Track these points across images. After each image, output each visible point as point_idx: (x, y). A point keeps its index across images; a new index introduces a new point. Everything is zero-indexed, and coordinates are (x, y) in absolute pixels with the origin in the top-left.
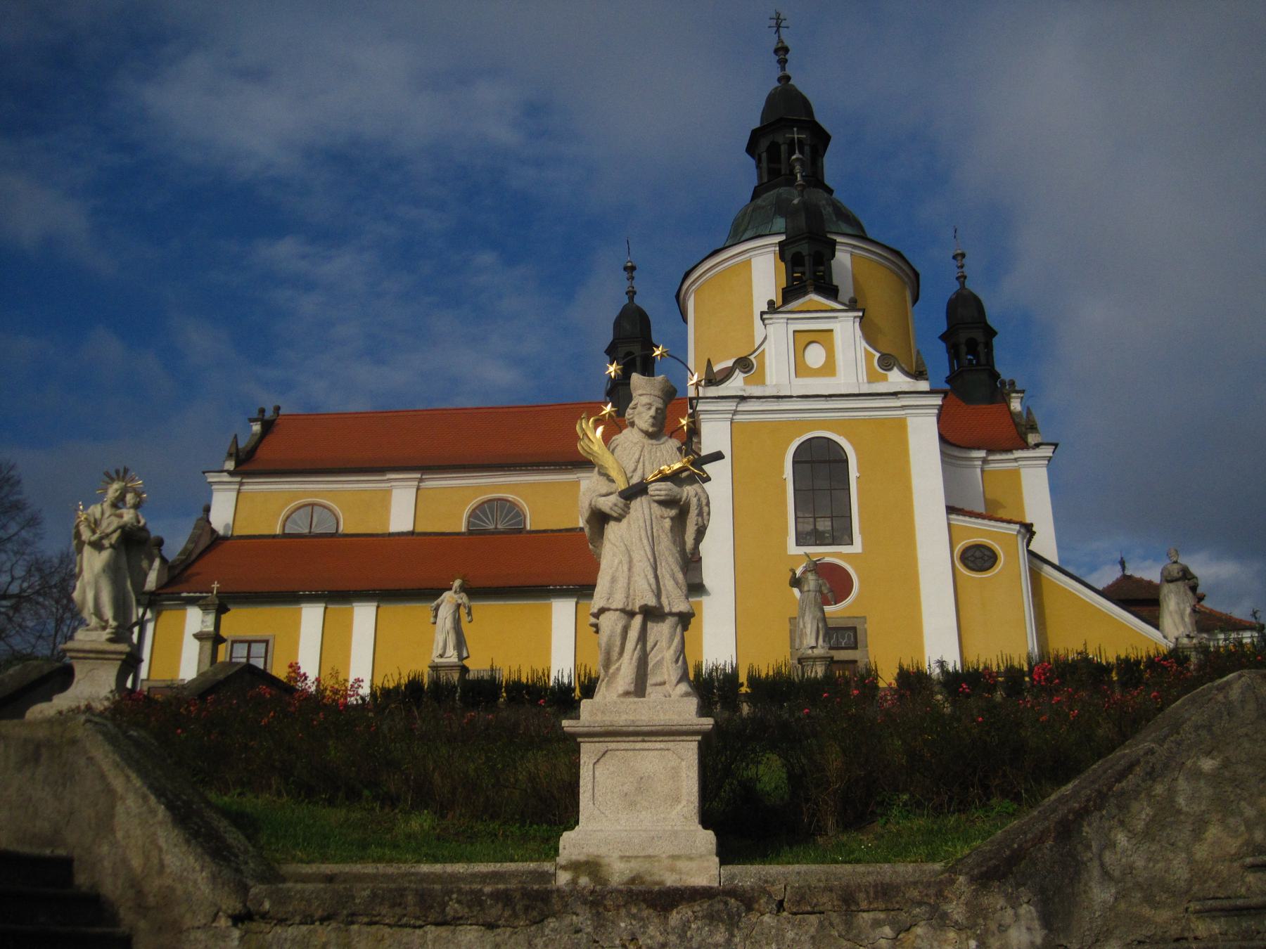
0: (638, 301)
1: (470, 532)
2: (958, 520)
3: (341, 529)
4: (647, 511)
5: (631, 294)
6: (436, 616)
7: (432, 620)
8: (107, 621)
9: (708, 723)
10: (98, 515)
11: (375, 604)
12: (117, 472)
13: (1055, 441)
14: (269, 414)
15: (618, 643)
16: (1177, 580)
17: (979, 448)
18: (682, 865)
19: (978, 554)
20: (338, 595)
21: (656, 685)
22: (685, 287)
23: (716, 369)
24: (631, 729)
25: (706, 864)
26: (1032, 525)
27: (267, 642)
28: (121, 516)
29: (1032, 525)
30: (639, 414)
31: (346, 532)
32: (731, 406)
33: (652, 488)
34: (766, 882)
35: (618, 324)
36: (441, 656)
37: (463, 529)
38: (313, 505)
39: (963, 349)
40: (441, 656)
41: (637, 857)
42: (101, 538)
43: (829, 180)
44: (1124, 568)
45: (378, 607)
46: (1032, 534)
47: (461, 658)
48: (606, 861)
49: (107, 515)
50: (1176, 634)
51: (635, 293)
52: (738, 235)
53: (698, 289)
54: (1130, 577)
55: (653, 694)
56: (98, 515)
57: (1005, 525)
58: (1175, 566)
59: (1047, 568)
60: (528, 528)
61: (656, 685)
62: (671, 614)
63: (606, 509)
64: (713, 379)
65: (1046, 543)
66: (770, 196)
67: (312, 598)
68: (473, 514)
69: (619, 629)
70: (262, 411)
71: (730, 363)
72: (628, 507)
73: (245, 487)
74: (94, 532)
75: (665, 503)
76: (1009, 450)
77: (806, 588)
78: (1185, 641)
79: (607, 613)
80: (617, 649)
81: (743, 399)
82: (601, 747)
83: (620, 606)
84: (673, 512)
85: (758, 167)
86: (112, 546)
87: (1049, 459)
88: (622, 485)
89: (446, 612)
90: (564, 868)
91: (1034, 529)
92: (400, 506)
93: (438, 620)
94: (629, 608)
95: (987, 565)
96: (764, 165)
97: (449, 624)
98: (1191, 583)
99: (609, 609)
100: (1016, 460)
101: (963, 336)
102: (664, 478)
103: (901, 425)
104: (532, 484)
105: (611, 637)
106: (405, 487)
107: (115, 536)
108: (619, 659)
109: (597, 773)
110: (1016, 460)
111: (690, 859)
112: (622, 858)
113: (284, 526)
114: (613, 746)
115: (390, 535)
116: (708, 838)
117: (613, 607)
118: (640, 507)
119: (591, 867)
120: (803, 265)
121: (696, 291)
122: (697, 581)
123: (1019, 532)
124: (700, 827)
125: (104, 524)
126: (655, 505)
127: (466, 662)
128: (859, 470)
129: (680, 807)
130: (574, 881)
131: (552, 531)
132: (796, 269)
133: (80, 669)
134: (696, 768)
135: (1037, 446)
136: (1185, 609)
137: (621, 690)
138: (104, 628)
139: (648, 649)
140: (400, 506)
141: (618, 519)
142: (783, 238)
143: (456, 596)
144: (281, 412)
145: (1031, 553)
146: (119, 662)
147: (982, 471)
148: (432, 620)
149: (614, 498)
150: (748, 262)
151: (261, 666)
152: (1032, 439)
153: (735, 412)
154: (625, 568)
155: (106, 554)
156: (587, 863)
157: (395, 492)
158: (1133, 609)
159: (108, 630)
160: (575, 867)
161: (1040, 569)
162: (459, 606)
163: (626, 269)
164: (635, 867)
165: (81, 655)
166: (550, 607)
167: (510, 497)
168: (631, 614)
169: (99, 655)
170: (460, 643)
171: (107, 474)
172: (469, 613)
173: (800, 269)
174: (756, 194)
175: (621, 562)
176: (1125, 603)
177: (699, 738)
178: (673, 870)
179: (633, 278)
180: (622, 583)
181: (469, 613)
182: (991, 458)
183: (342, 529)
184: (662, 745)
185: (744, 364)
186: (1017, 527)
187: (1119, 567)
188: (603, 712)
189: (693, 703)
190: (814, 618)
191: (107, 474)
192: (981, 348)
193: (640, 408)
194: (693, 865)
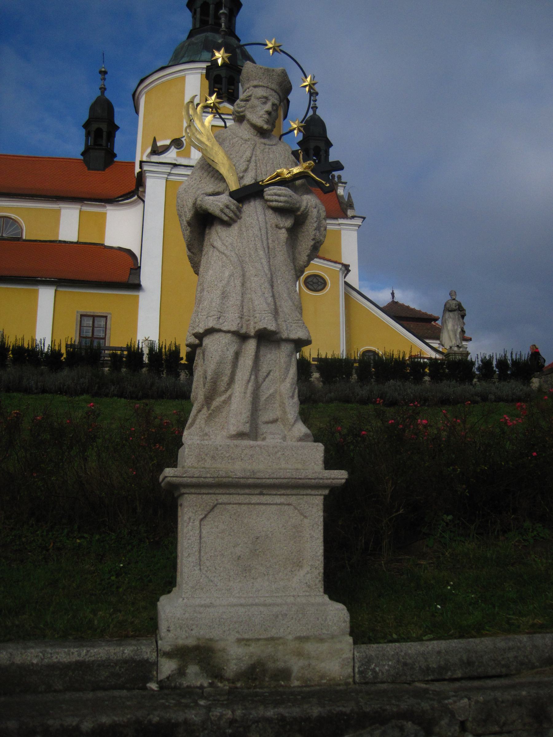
0: (107, 95)
4: (261, 218)
5: (103, 89)
9: (340, 476)
15: (228, 372)
16: (454, 310)
18: (310, 647)
19: (315, 280)
21: (267, 423)
22: (139, 89)
23: (159, 144)
24: (250, 481)
25: (338, 646)
26: (349, 266)
29: (349, 266)
30: (253, 107)
32: (167, 169)
33: (269, 193)
34: (405, 664)
35: (93, 108)
39: (312, 152)
41: (259, 640)
43: (238, 33)
46: (348, 271)
48: (221, 645)
50: (451, 344)
51: (105, 89)
52: (178, 58)
53: (148, 91)
54: (397, 303)
55: (272, 438)
58: (454, 302)
60: (24, 238)
61: (267, 423)
62: (288, 340)
63: (216, 211)
64: (156, 151)
66: (201, 37)
69: (230, 354)
71: (168, 142)
72: (239, 210)
75: (280, 211)
76: (336, 218)
78: (456, 349)
79: (217, 336)
80: (226, 379)
81: (175, 165)
82: (210, 500)
83: (234, 328)
84: (289, 223)
85: (194, 17)
87: (359, 226)
88: (234, 186)
90: (169, 655)
94: (243, 331)
95: (320, 288)
96: (198, 16)
98: (462, 313)
99: (219, 331)
100: (339, 224)
101: (312, 145)
102: (284, 182)
105: (220, 363)
108: (226, 390)
109: (204, 532)
111: (321, 640)
112: (239, 641)
114: (223, 499)
115: (60, 241)
116: (337, 614)
117: (225, 329)
118: (253, 212)
119: (201, 654)
120: (221, 84)
121: (146, 93)
122: (137, 282)
123: (341, 269)
124: (326, 597)
126: (270, 213)
129: (302, 573)
130: (181, 672)
131: (40, 241)
132: (216, 85)
134: (321, 528)
135: (353, 217)
136: (457, 329)
137: (233, 430)
139: (260, 380)
141: (227, 224)
142: (209, 64)
145: (346, 283)
149: (225, 199)
150: (183, 78)
152: (350, 213)
153: (169, 174)
154: (238, 283)
156: (197, 648)
158: (401, 322)
160: (182, 653)
163: (101, 72)
164: (256, 651)
166: (37, 291)
167: (13, 216)
168: (243, 337)
173: (219, 86)
174: (191, 35)
175: (231, 276)
176: (398, 319)
177: (326, 492)
178: (300, 654)
179: (104, 79)
180: (234, 299)
184: (282, 499)
185: (177, 143)
186: (340, 266)
188: (213, 458)
189: (317, 451)
192: (322, 153)
193: (254, 101)
194: (325, 647)
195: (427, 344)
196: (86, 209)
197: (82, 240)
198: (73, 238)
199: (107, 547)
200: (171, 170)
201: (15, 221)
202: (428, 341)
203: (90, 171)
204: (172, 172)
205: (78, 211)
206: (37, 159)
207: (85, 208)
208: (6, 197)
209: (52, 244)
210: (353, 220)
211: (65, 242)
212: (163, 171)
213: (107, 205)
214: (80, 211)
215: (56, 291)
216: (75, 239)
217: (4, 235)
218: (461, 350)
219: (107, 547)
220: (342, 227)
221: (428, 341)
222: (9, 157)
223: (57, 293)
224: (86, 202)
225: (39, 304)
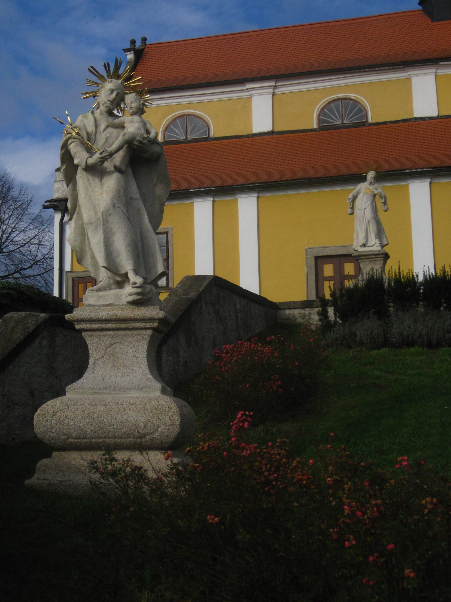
1: (321, 128)
3: (212, 134)
6: (352, 208)
7: (349, 211)
8: (126, 276)
10: (91, 128)
11: (256, 195)
12: (107, 67)
14: (138, 45)
20: (223, 190)
27: (167, 233)
28: (122, 127)
31: (216, 136)
36: (364, 245)
37: (315, 126)
38: (187, 115)
40: (364, 245)
42: (103, 160)
47: (383, 246)
49: (102, 126)
56: (91, 128)
60: (370, 121)
68: (322, 112)
70: (133, 42)
73: (278, 91)
74: (90, 151)
86: (118, 169)
89: (363, 204)
92: (260, 110)
93: (357, 211)
97: (369, 214)
104: (370, 84)
107: (118, 158)
113: (164, 135)
115: (416, 119)
125: (101, 140)
127: (386, 249)
131: (391, 122)
133: (95, 345)
138: (120, 285)
140: (260, 110)
143: (371, 187)
144: (148, 42)
146: (150, 332)
148: (349, 211)
151: (258, 293)
155: (111, 182)
157: (254, 99)
159: (128, 289)
162: (374, 196)
165: (96, 326)
166: (407, 187)
167: (353, 96)
169: (119, 325)
170: (380, 233)
171: (93, 71)
172: (385, 203)
181: (385, 203)
183: (212, 134)
191: (93, 71)
196: (443, 72)
199: (405, 482)
200: (276, 83)
201: (355, 102)
203: (435, 23)
204: (278, 84)
205: (433, 76)
206: (366, 20)
209: (405, 124)
211: (422, 119)
212: (262, 86)
214: (436, 76)
215: (431, 183)
216: (435, 113)
217: (345, 122)
219: (405, 482)
222: (331, 24)
223: (432, 185)
224: (441, 63)
225: (411, 204)
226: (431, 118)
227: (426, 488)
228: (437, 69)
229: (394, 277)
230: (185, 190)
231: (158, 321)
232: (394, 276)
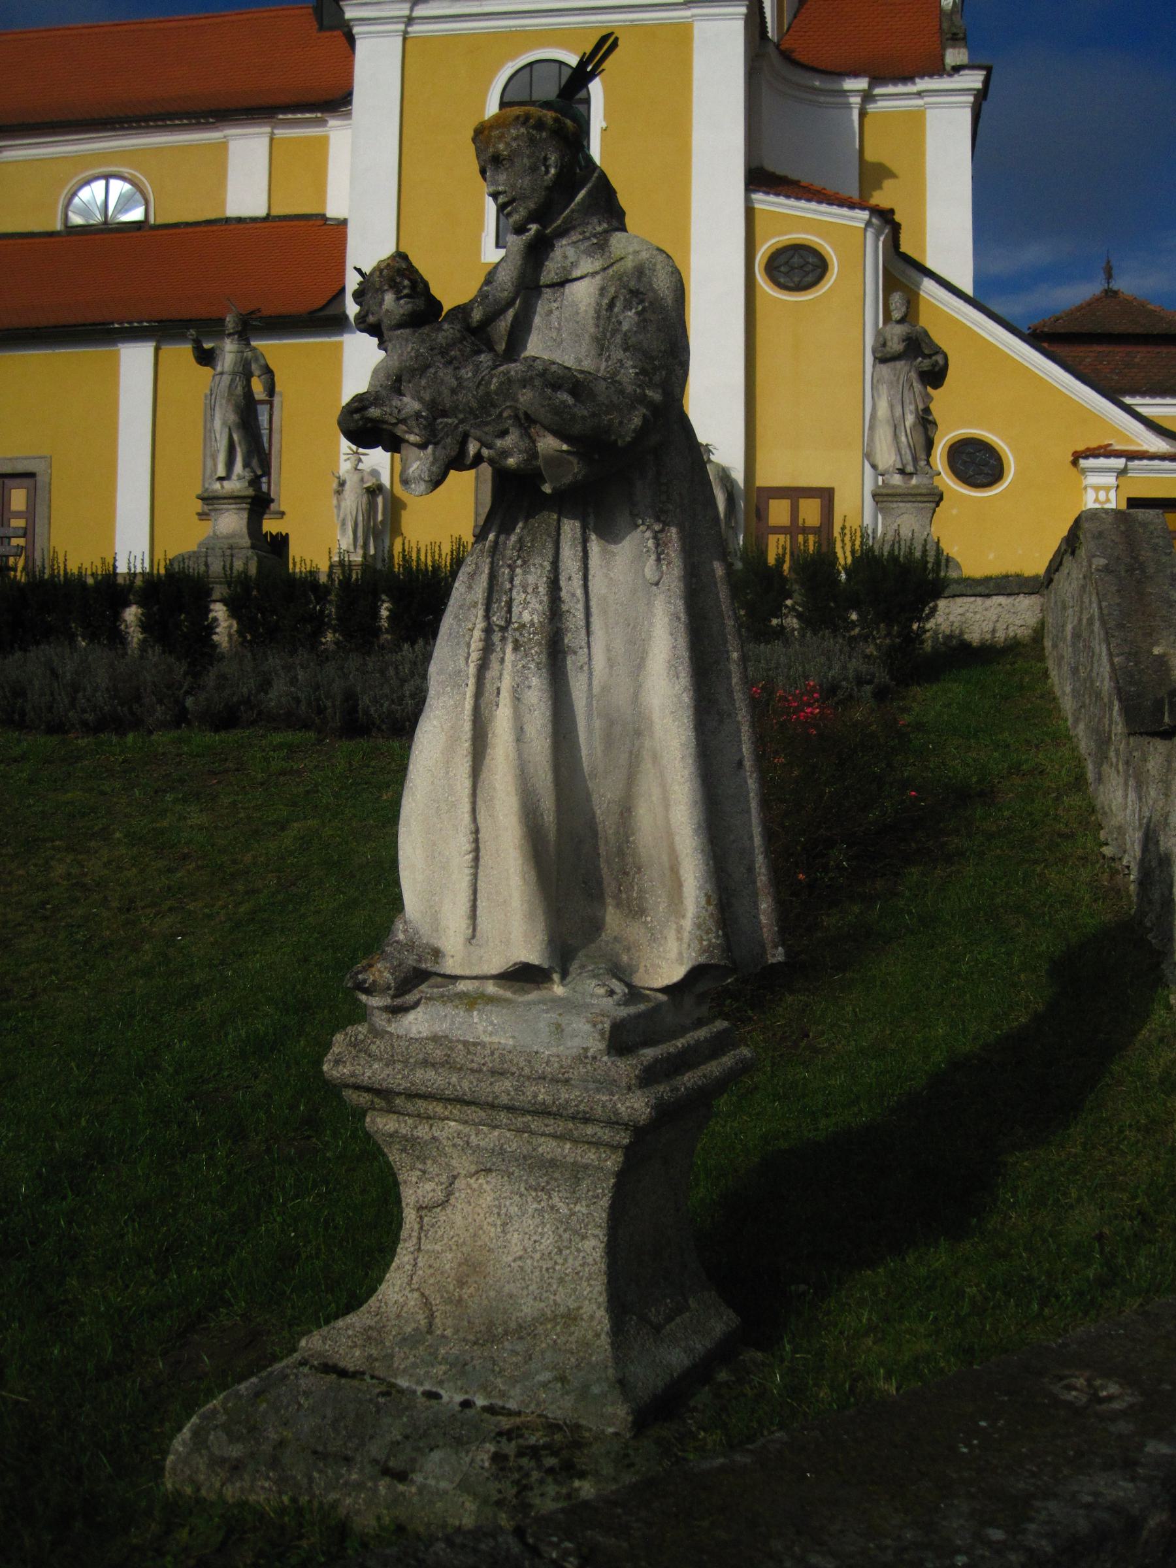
2: (765, 202)
13: (987, 63)
17: (856, 74)
26: (892, 211)
29: (892, 211)
44: (1109, 276)
45: (157, 350)
54: (1116, 293)
57: (845, 211)
59: (928, 284)
65: (947, 237)
67: (135, 334)
76: (908, 78)
77: (219, 369)
78: (897, 479)
91: (897, 218)
95: (809, 279)
100: (919, 94)
103: (682, 36)
104: (158, 150)
106: (951, 105)
110: (919, 94)
115: (228, 220)
123: (868, 224)
128: (607, 117)
131: (187, 224)
135: (957, 69)
147: (863, 114)
161: (918, 285)
182: (878, 91)
186: (865, 215)
187: (1102, 276)
190: (224, 423)
195: (1129, 410)
197: (276, 212)
198: (258, 208)
200: (412, 10)
202: (1128, 400)
204: (416, 14)
205: (265, 141)
207: (280, 133)
208: (97, 131)
210: (956, 78)
211: (240, 220)
213: (326, 116)
214: (272, 140)
216: (261, 212)
218: (914, 481)
220: (927, 100)
221: (1128, 400)
226: (254, 220)
227: (984, 1428)
228: (273, 128)
229: (886, 554)
230: (103, 324)
231: (824, 549)
232: (429, 563)
